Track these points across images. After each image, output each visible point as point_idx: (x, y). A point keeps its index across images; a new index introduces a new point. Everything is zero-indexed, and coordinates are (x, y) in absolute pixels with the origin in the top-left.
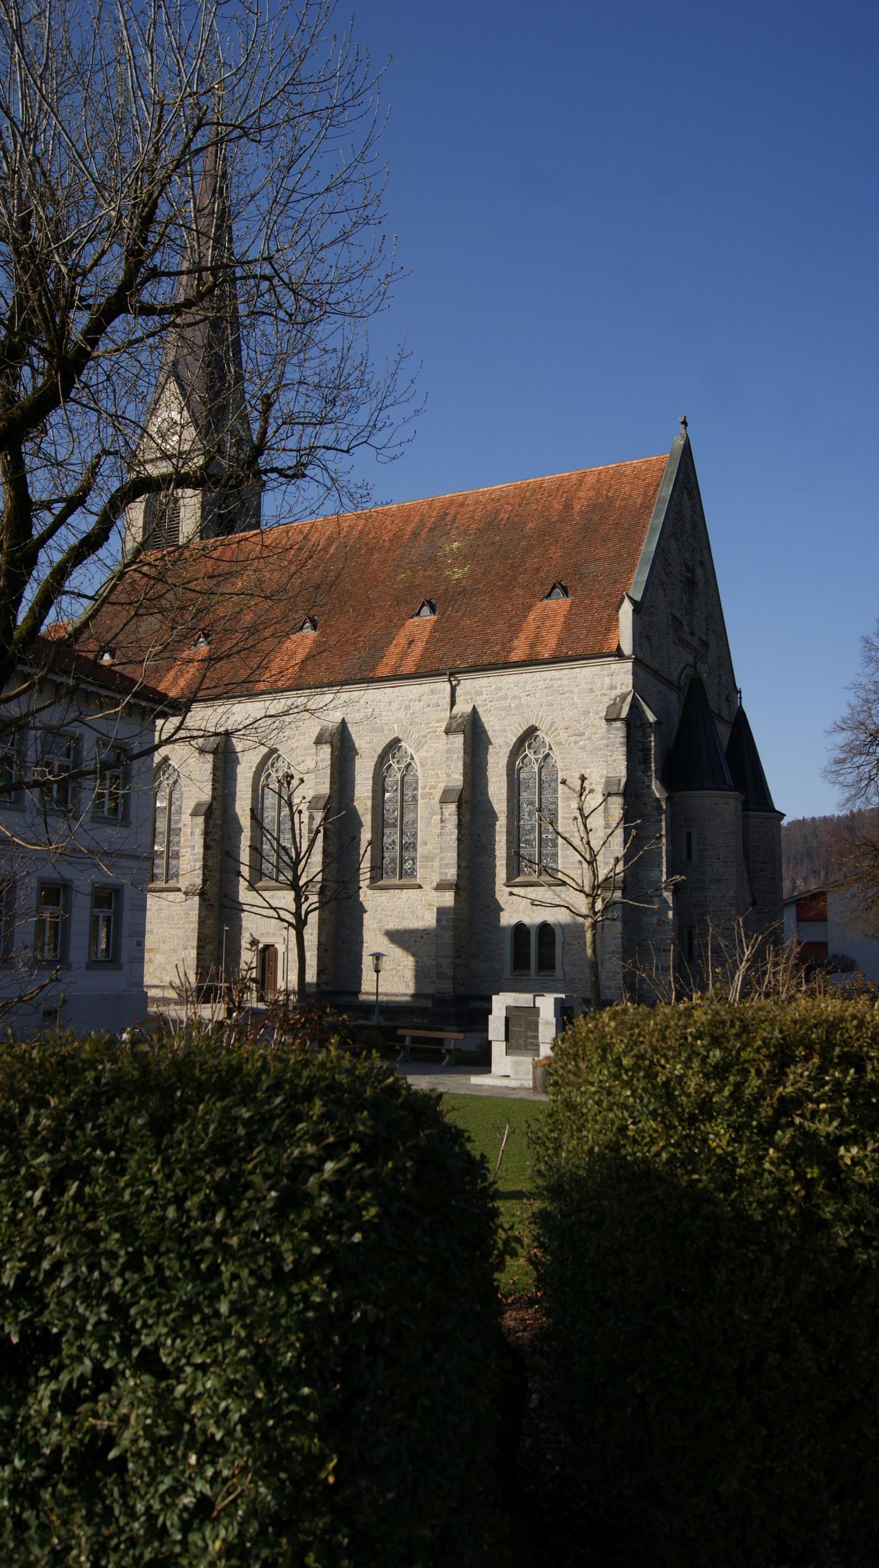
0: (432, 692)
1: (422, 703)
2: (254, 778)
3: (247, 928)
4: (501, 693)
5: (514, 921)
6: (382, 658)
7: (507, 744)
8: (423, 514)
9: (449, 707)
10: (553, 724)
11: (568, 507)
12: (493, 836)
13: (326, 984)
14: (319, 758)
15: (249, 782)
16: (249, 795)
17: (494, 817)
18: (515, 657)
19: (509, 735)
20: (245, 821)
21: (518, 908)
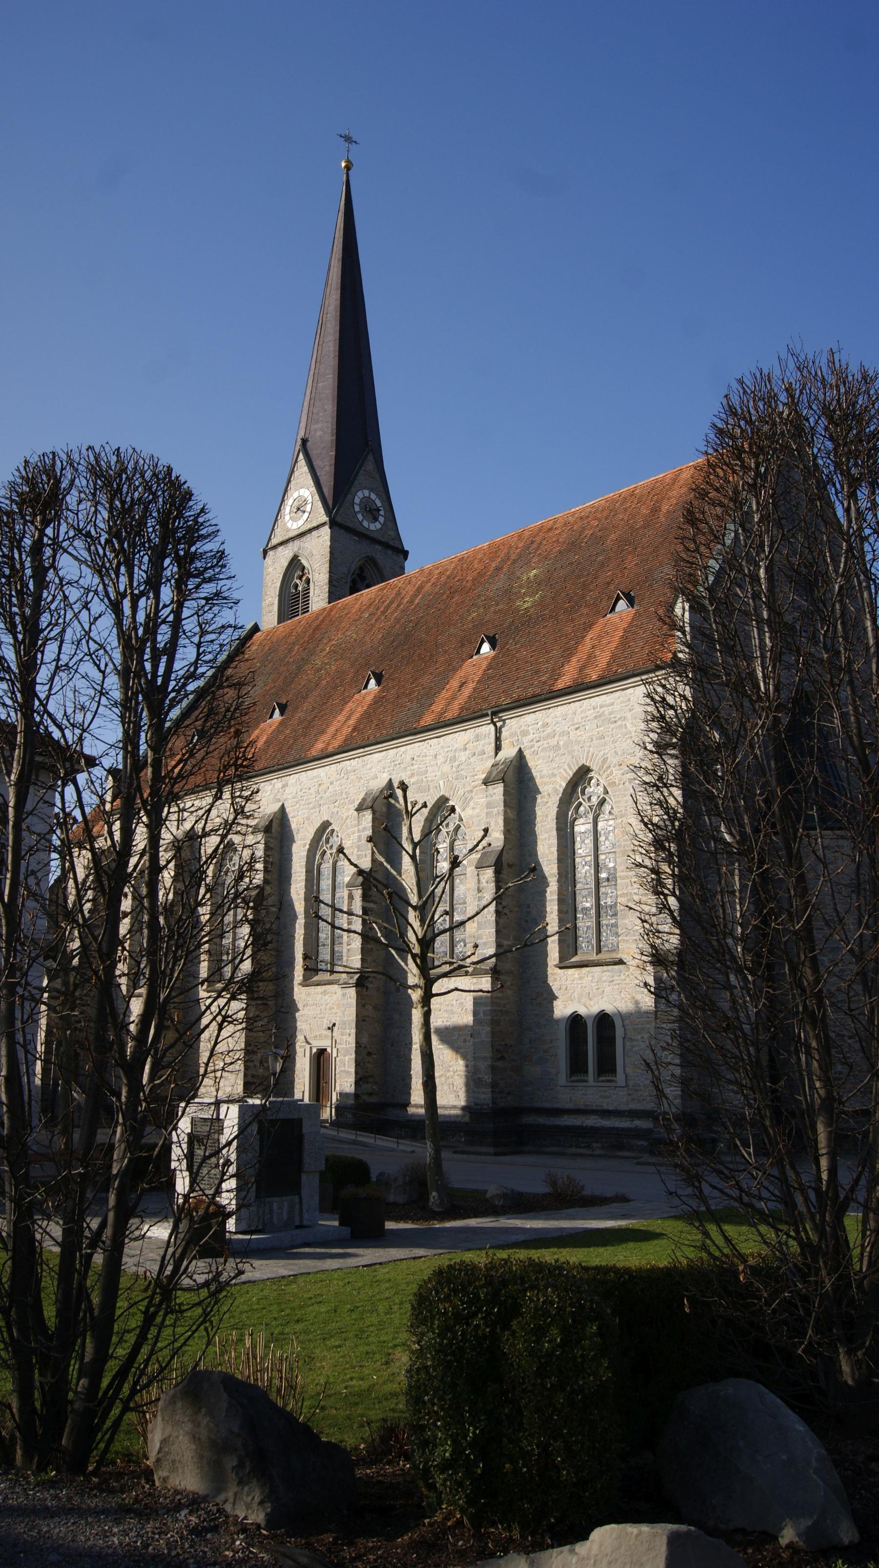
0: (477, 738)
1: (467, 752)
2: (308, 857)
3: (301, 1030)
4: (549, 730)
5: (568, 1011)
6: (431, 705)
7: (556, 790)
8: (511, 547)
9: (493, 753)
10: (605, 760)
11: (655, 510)
12: (544, 906)
13: (370, 1094)
14: (361, 827)
15: (303, 862)
16: (303, 877)
17: (543, 881)
18: (560, 685)
19: (558, 779)
20: (299, 907)
21: (576, 992)
